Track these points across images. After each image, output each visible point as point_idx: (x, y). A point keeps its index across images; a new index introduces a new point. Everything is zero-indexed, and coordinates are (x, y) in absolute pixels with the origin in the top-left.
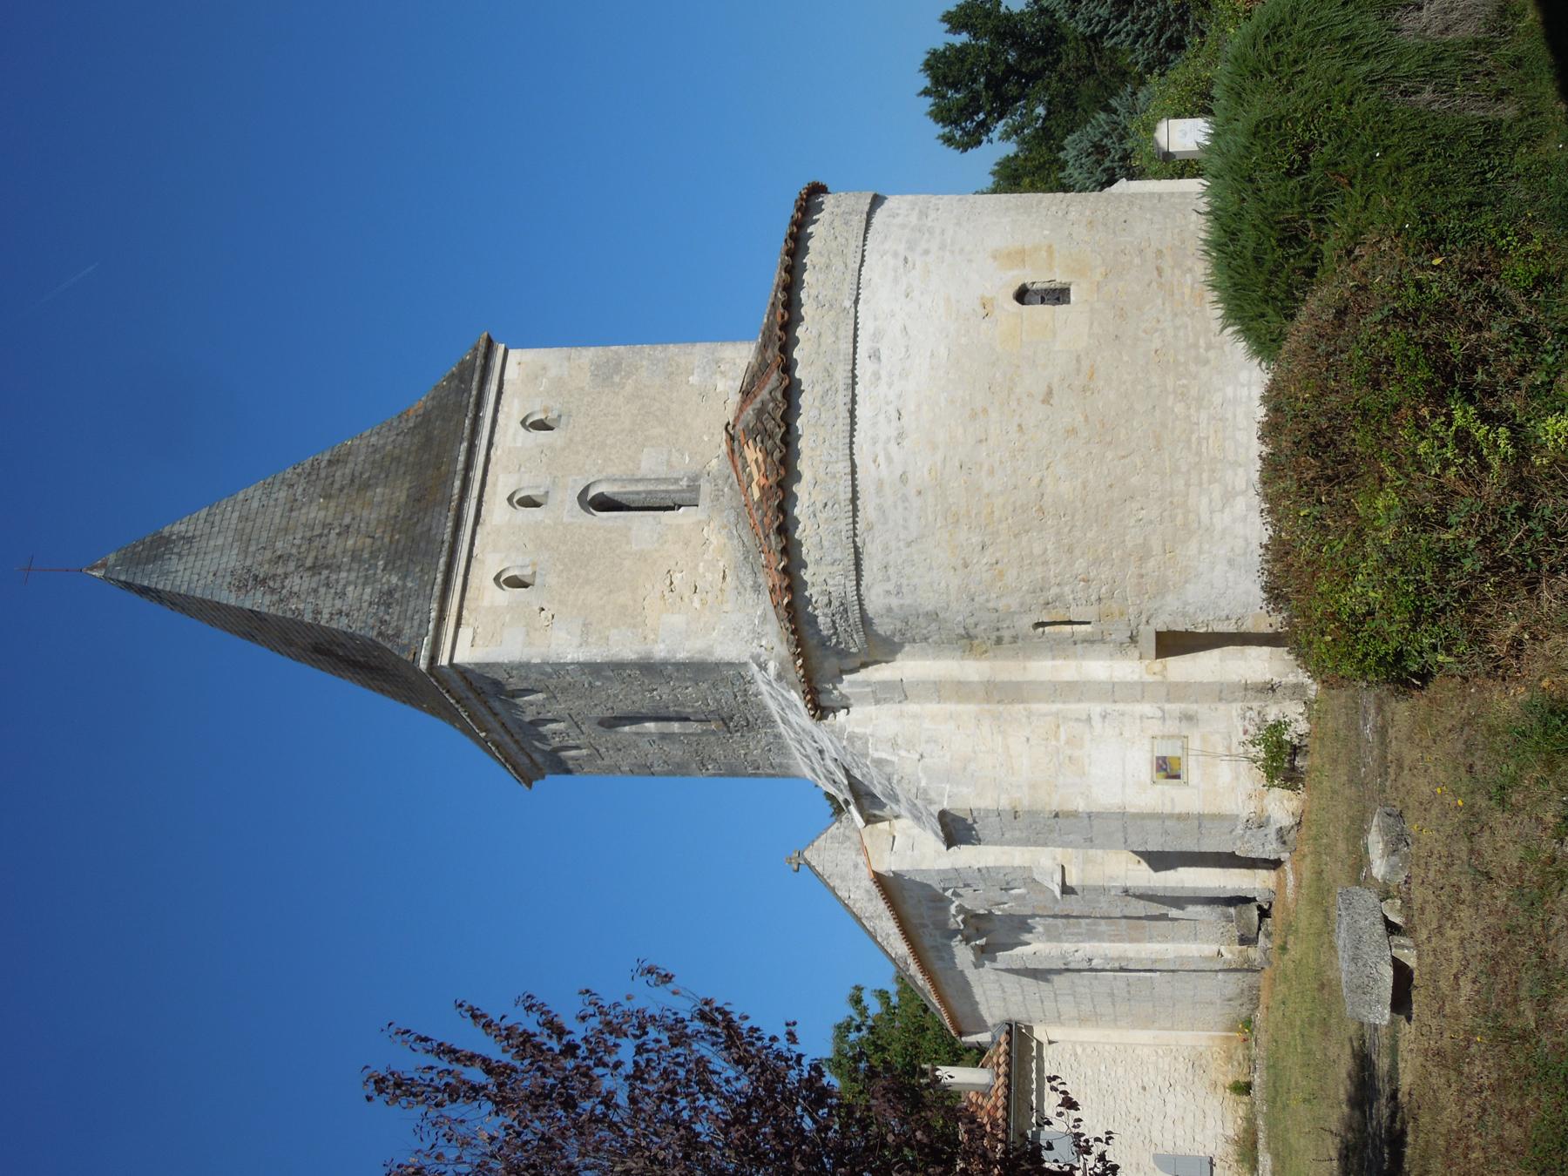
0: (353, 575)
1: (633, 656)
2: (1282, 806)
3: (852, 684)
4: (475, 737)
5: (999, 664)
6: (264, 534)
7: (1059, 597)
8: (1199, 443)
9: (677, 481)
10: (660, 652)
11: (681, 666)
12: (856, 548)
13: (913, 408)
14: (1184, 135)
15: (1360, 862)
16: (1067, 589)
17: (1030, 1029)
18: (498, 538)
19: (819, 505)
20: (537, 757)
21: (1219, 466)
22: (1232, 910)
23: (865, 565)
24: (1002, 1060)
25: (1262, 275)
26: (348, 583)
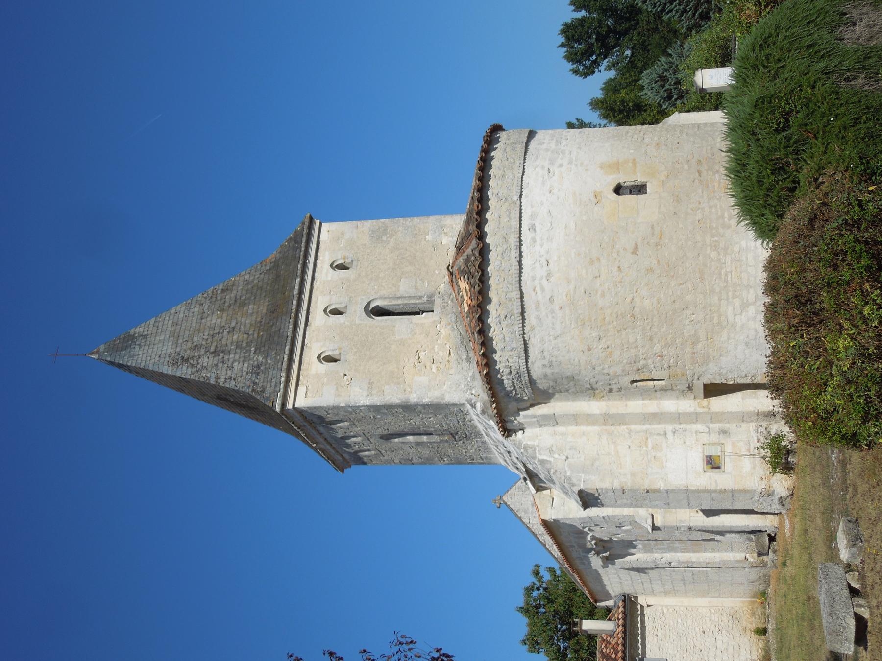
0: (237, 356)
1: (398, 402)
2: (781, 484)
3: (525, 417)
4: (311, 446)
5: (610, 403)
6: (187, 333)
7: (645, 366)
8: (726, 275)
9: (421, 297)
10: (413, 398)
11: (426, 406)
12: (525, 341)
13: (555, 258)
14: (715, 78)
15: (833, 555)
16: (650, 361)
17: (636, 598)
18: (319, 333)
19: (502, 317)
20: (347, 456)
21: (738, 288)
22: (752, 536)
23: (531, 350)
24: (620, 616)
25: (764, 186)
26: (234, 361)
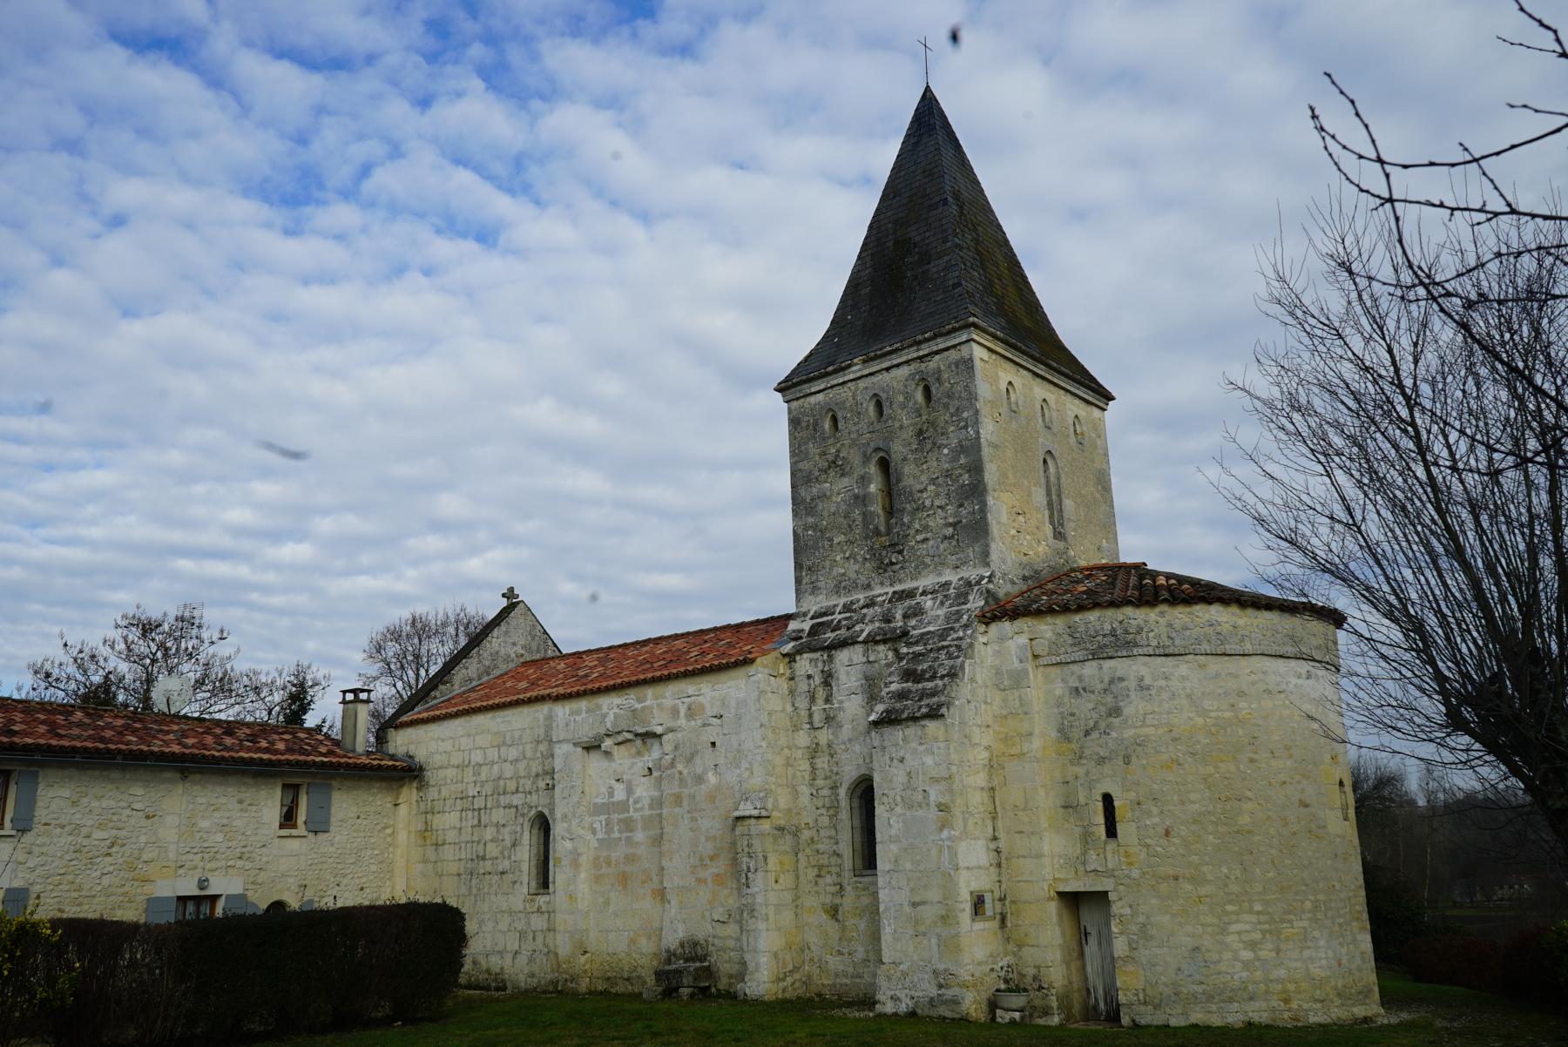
19: (1219, 629)
23: (1281, 661)
